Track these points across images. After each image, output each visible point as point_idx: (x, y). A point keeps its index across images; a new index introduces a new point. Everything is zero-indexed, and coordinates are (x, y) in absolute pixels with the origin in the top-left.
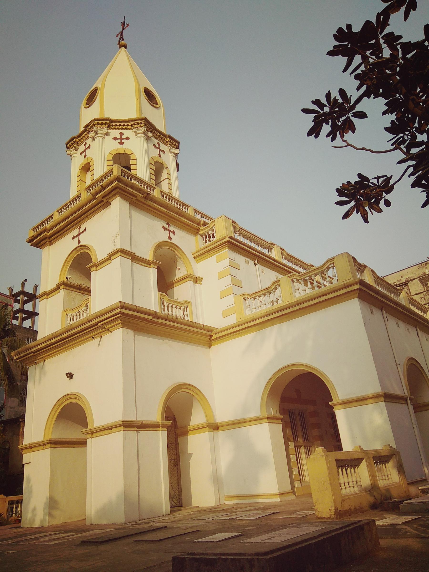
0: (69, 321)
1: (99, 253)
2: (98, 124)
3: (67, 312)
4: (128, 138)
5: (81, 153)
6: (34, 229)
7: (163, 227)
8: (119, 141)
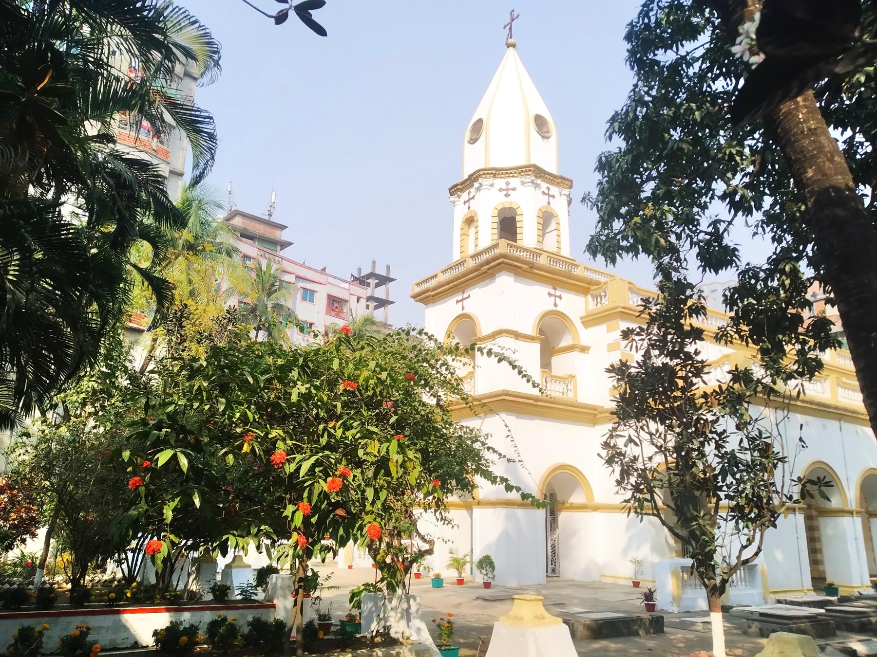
4: (514, 189)
5: (465, 203)
6: (417, 285)
8: (505, 192)
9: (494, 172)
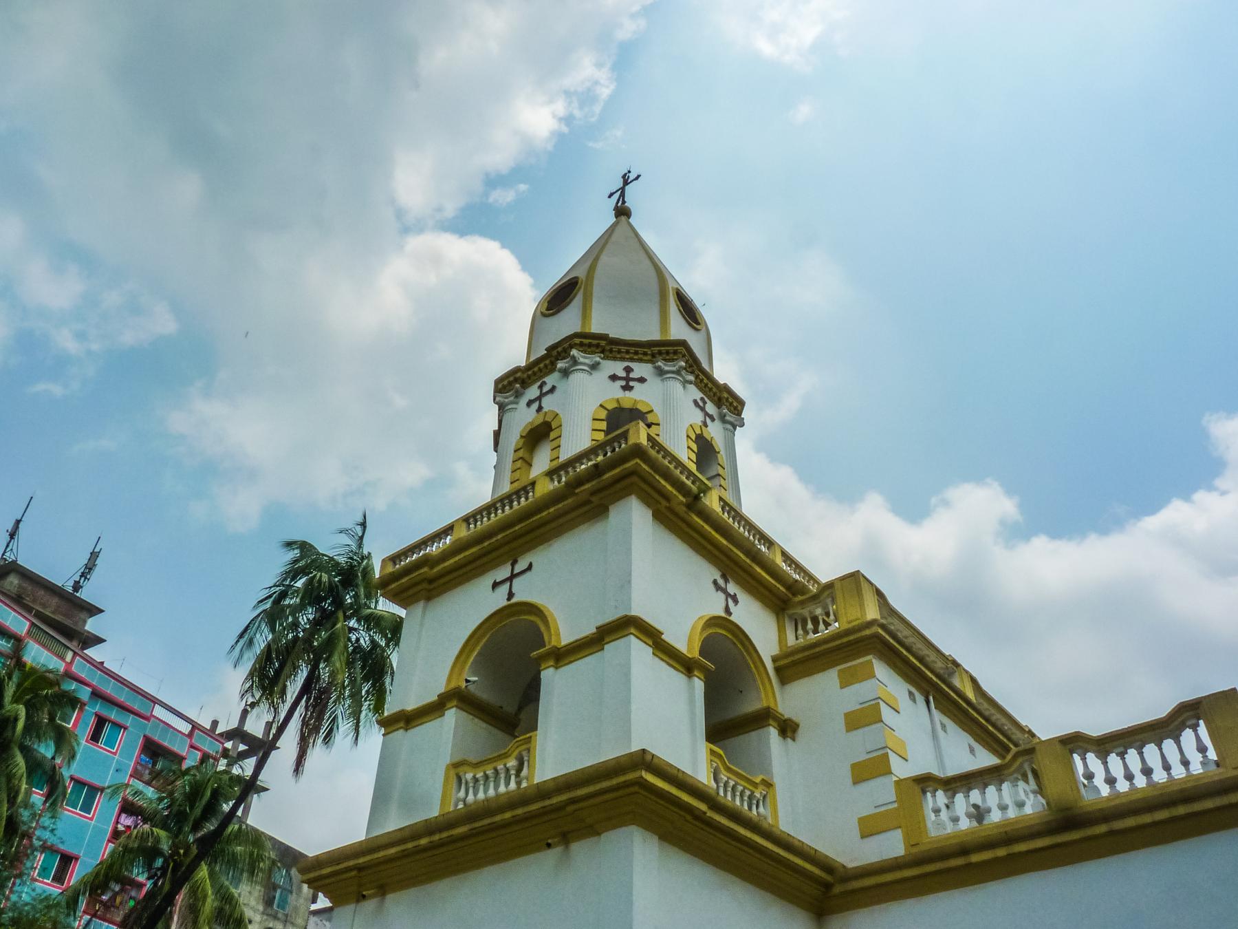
0: (462, 794)
1: (567, 628)
2: (706, 385)
3: (461, 770)
4: (642, 380)
5: (529, 404)
7: (715, 582)
9: (603, 343)
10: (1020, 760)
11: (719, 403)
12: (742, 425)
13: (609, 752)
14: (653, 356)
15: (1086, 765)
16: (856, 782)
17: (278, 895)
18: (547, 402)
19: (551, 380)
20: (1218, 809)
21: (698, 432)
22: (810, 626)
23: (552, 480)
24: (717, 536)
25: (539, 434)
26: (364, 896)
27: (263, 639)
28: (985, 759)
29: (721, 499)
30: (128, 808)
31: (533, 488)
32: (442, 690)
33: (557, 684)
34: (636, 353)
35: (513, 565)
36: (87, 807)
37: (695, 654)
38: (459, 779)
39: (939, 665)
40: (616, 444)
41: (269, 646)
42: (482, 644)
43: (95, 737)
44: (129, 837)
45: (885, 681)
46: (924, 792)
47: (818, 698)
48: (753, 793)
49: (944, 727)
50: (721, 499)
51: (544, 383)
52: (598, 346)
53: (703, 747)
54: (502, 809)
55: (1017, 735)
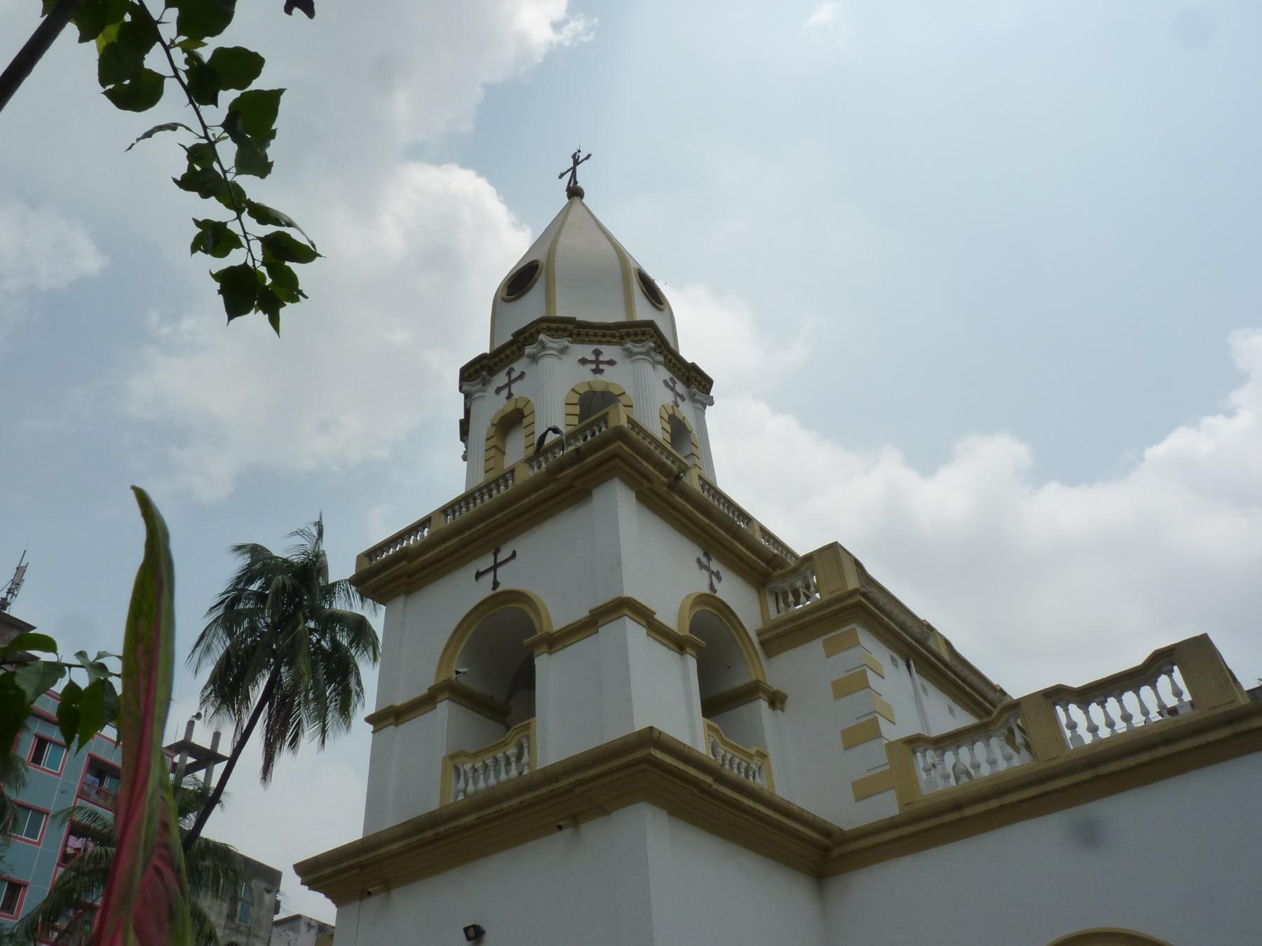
0: (461, 785)
4: (611, 363)
7: (699, 561)
8: (593, 366)
9: (570, 327)
10: (1006, 715)
11: (688, 382)
12: (712, 404)
13: (613, 732)
14: (621, 338)
15: (1068, 716)
16: (847, 747)
17: (239, 908)
18: (517, 389)
19: (519, 366)
20: (1197, 748)
21: (671, 412)
22: (791, 599)
23: (532, 466)
24: (701, 516)
25: (511, 421)
26: (369, 893)
27: (220, 647)
28: (965, 720)
29: (700, 478)
30: (77, 830)
31: (513, 475)
32: (432, 683)
33: (550, 671)
34: (604, 335)
35: (495, 555)
36: (32, 832)
37: (684, 631)
38: (457, 770)
39: (916, 630)
40: (596, 428)
41: (228, 653)
42: (471, 631)
43: (37, 758)
44: (82, 859)
45: (870, 648)
46: (914, 753)
47: (804, 669)
48: (749, 764)
49: (924, 689)
50: (700, 478)
51: (511, 370)
52: (565, 330)
53: (700, 721)
54: (508, 796)
55: (991, 695)
